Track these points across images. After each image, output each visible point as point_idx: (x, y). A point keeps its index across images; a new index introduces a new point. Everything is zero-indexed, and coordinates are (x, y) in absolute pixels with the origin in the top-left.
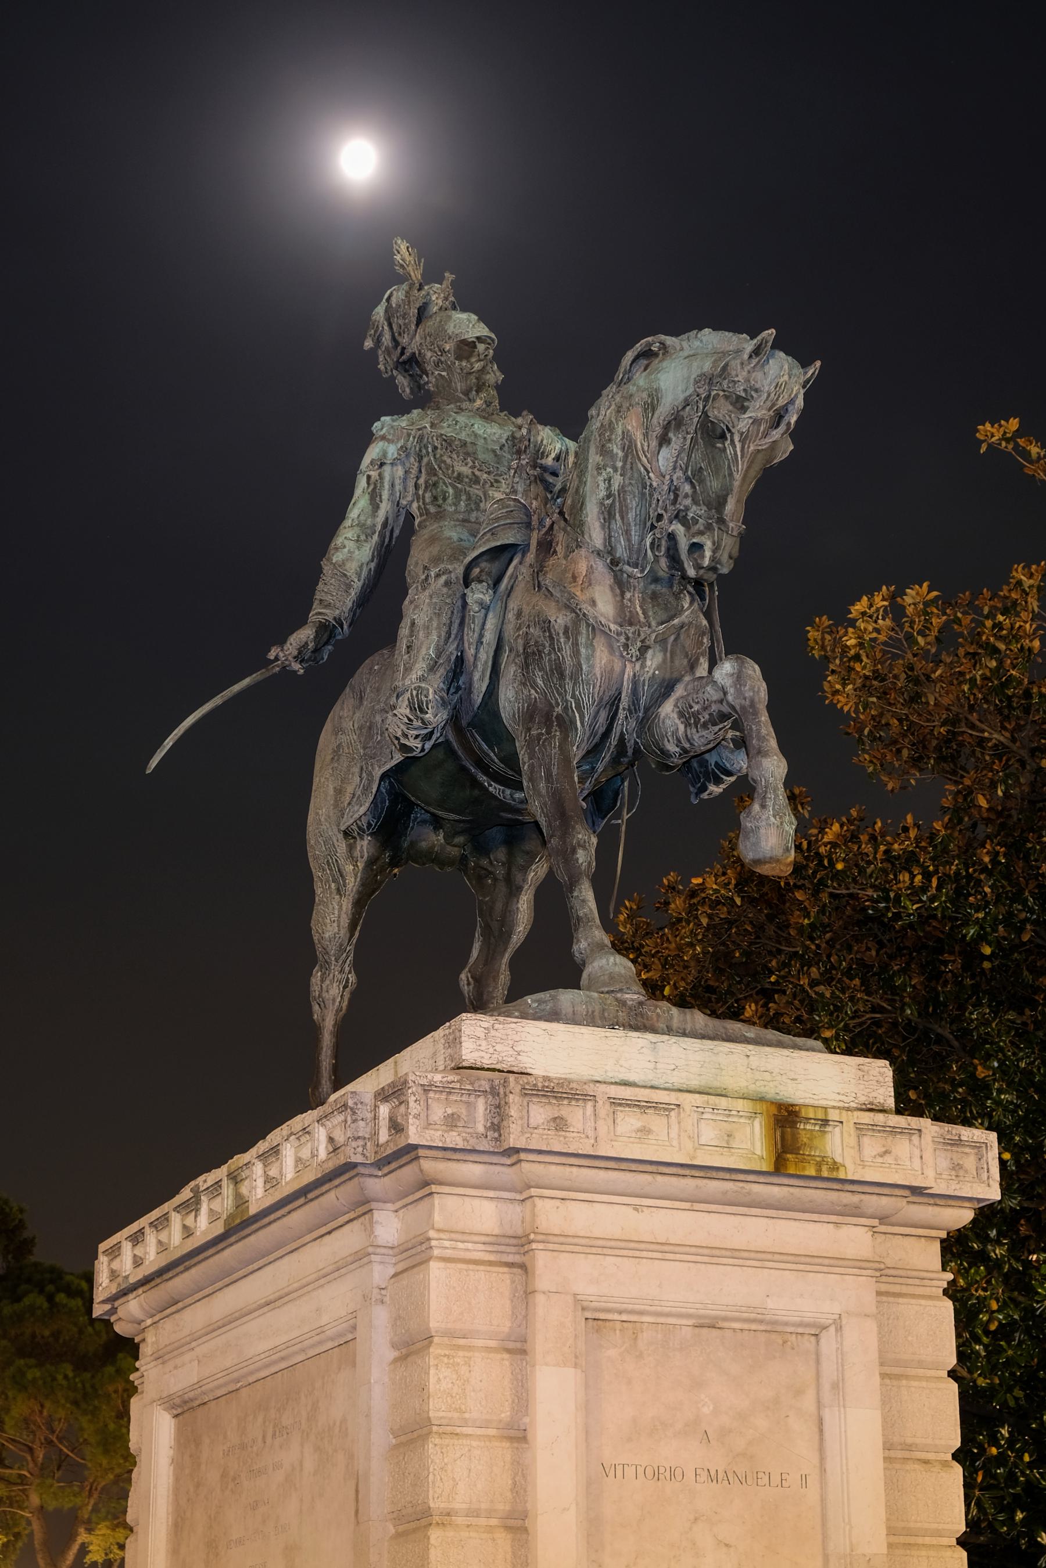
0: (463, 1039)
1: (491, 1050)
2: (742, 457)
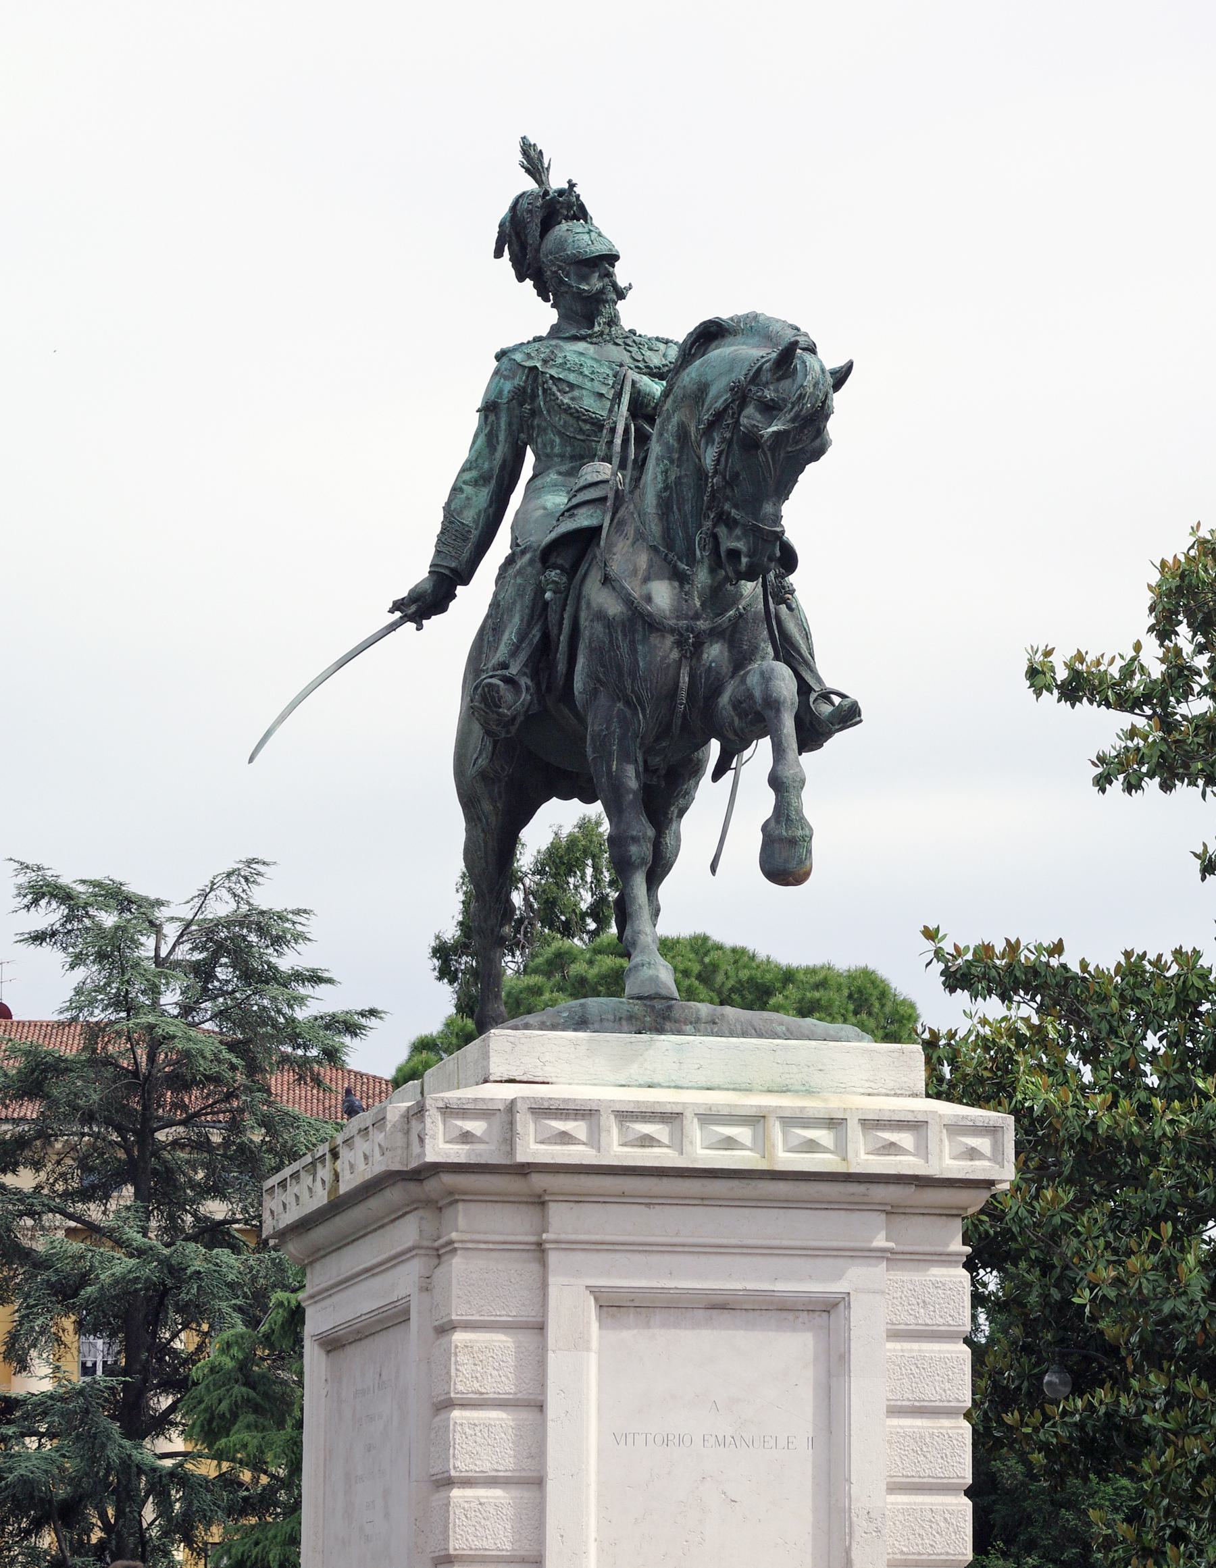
2: (774, 464)
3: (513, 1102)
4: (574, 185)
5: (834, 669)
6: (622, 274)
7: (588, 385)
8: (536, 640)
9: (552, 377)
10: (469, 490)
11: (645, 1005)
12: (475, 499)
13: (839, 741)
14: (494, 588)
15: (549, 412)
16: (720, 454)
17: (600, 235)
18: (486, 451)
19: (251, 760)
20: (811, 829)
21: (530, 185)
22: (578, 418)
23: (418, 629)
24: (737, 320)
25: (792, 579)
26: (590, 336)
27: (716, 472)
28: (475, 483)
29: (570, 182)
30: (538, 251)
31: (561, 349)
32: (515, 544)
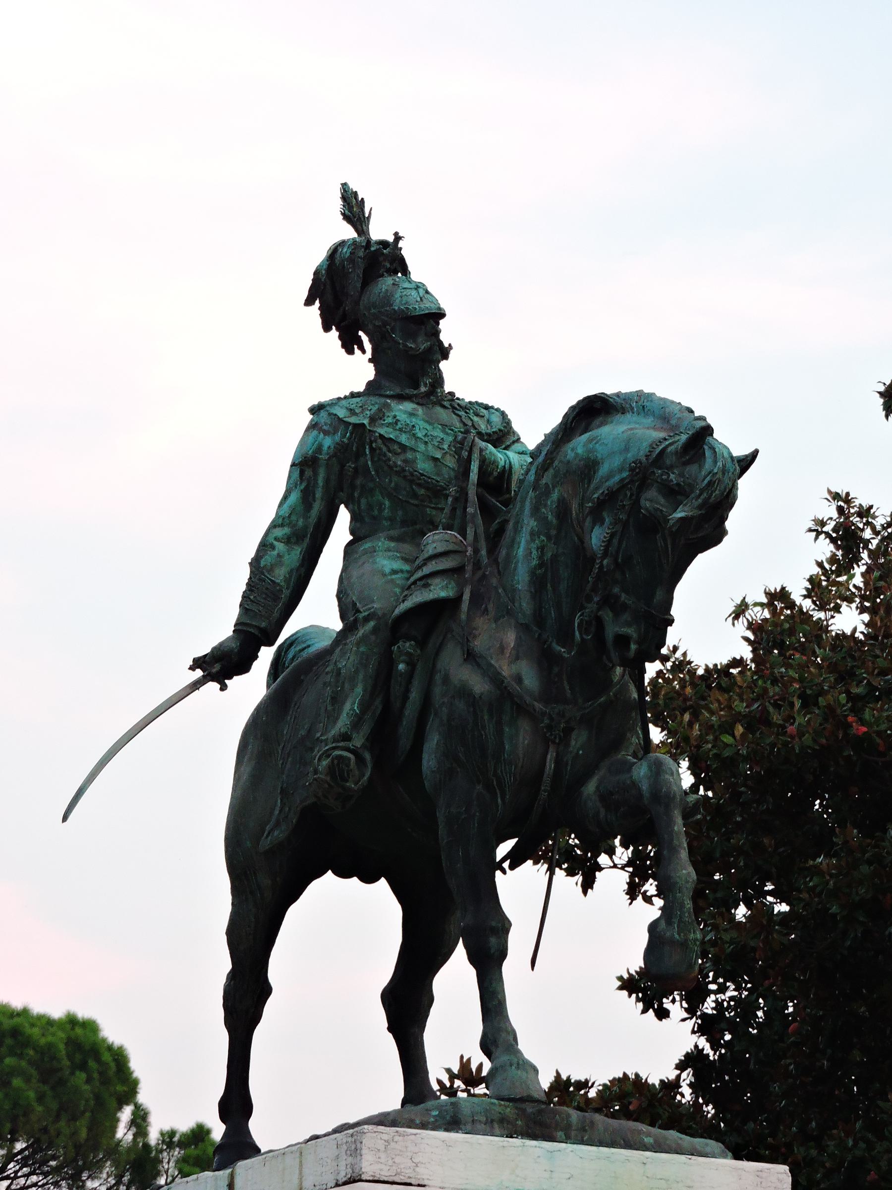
0: (363, 1152)
1: (390, 1162)
6: (447, 332)
7: (422, 447)
8: (378, 712)
9: (381, 436)
10: (280, 547)
11: (516, 1108)
12: (286, 557)
15: (377, 471)
16: (612, 535)
17: (427, 292)
18: (300, 508)
19: (65, 819)
21: (349, 233)
22: (411, 482)
23: (222, 689)
26: (416, 396)
27: (606, 554)
28: (288, 540)
29: (396, 234)
30: (357, 303)
31: (387, 406)
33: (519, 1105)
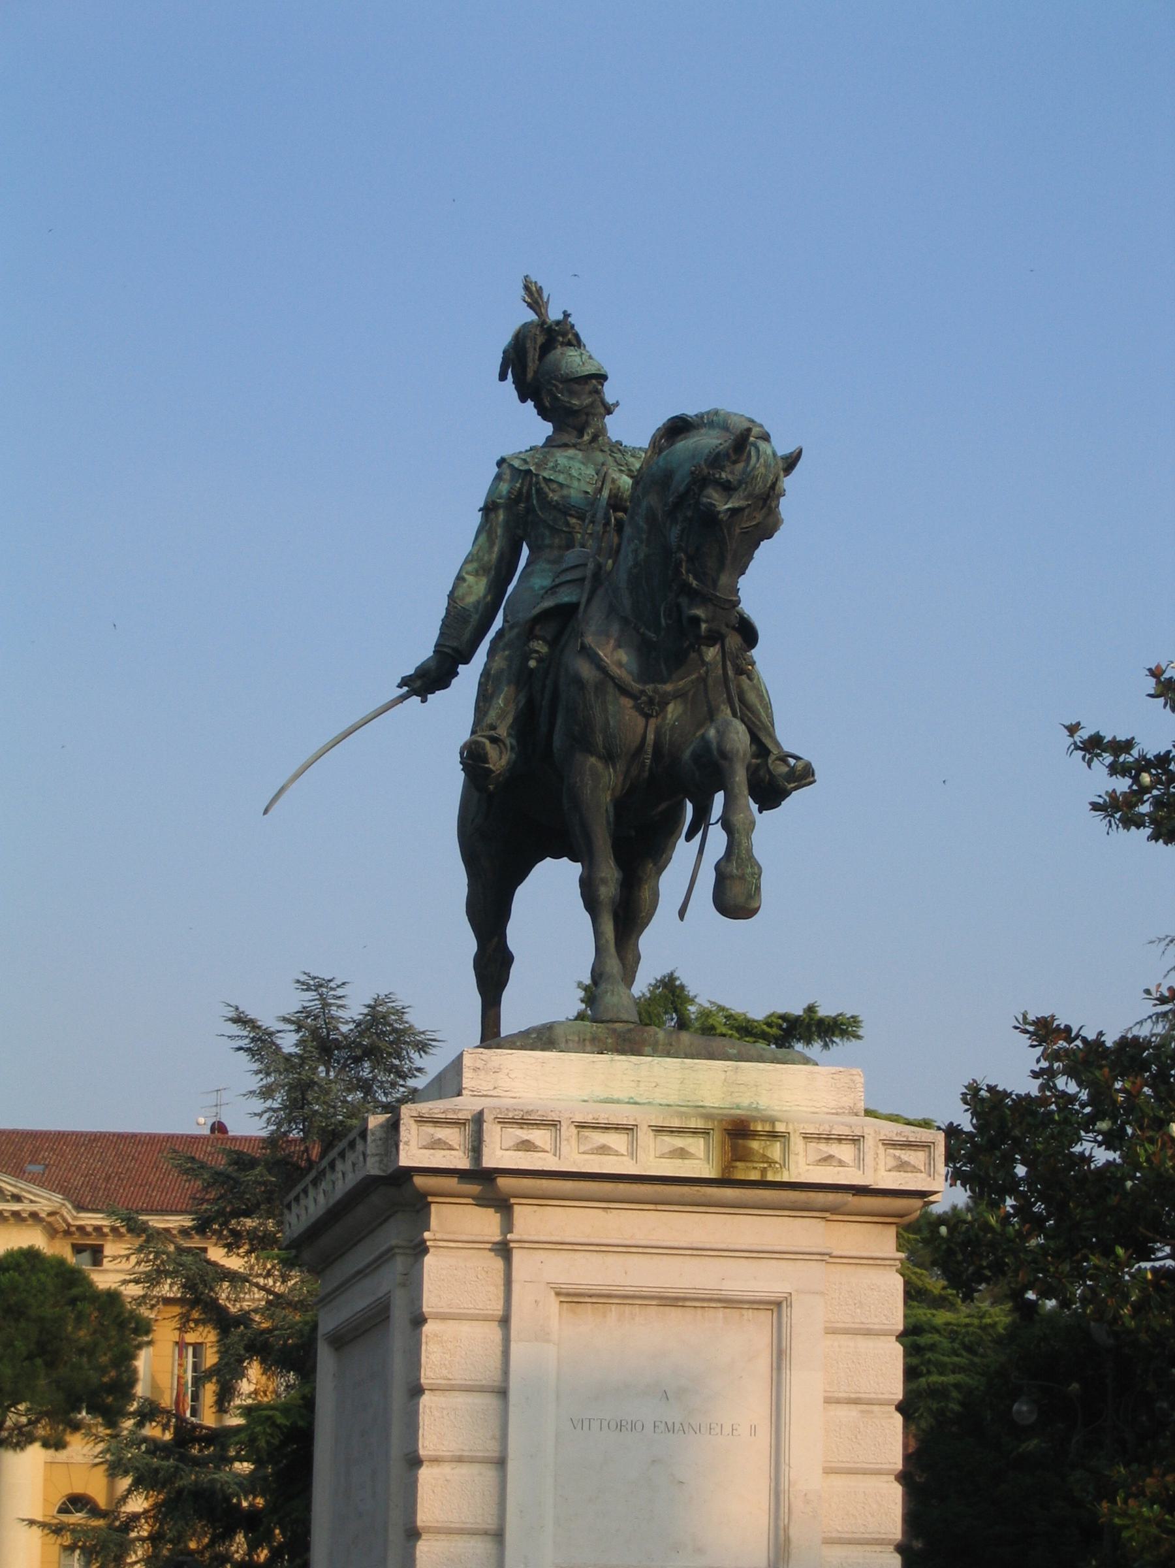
3: (481, 1113)
4: (569, 315)
5: (790, 735)
6: (610, 392)
9: (544, 478)
10: (470, 579)
13: (797, 800)
14: (485, 659)
17: (590, 357)
19: (266, 812)
20: (760, 868)
21: (531, 316)
24: (700, 416)
25: (755, 653)
28: (476, 573)
32: (505, 621)
33: (610, 1025)
